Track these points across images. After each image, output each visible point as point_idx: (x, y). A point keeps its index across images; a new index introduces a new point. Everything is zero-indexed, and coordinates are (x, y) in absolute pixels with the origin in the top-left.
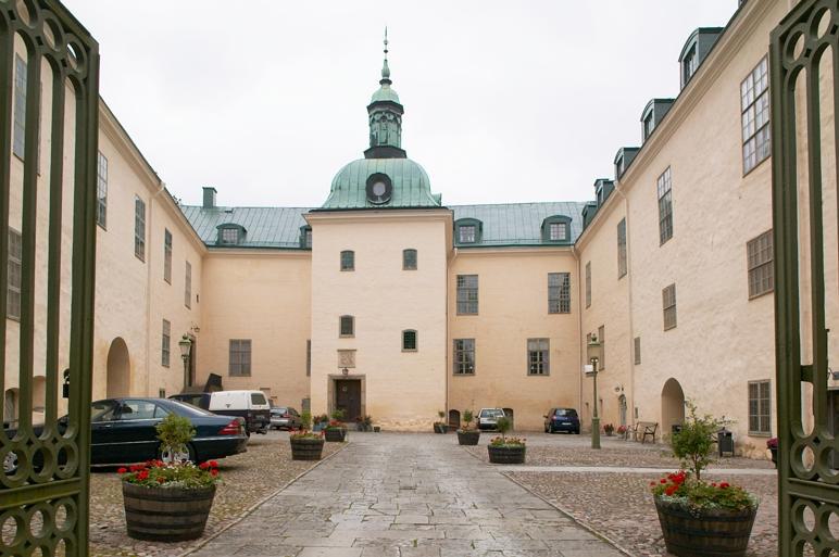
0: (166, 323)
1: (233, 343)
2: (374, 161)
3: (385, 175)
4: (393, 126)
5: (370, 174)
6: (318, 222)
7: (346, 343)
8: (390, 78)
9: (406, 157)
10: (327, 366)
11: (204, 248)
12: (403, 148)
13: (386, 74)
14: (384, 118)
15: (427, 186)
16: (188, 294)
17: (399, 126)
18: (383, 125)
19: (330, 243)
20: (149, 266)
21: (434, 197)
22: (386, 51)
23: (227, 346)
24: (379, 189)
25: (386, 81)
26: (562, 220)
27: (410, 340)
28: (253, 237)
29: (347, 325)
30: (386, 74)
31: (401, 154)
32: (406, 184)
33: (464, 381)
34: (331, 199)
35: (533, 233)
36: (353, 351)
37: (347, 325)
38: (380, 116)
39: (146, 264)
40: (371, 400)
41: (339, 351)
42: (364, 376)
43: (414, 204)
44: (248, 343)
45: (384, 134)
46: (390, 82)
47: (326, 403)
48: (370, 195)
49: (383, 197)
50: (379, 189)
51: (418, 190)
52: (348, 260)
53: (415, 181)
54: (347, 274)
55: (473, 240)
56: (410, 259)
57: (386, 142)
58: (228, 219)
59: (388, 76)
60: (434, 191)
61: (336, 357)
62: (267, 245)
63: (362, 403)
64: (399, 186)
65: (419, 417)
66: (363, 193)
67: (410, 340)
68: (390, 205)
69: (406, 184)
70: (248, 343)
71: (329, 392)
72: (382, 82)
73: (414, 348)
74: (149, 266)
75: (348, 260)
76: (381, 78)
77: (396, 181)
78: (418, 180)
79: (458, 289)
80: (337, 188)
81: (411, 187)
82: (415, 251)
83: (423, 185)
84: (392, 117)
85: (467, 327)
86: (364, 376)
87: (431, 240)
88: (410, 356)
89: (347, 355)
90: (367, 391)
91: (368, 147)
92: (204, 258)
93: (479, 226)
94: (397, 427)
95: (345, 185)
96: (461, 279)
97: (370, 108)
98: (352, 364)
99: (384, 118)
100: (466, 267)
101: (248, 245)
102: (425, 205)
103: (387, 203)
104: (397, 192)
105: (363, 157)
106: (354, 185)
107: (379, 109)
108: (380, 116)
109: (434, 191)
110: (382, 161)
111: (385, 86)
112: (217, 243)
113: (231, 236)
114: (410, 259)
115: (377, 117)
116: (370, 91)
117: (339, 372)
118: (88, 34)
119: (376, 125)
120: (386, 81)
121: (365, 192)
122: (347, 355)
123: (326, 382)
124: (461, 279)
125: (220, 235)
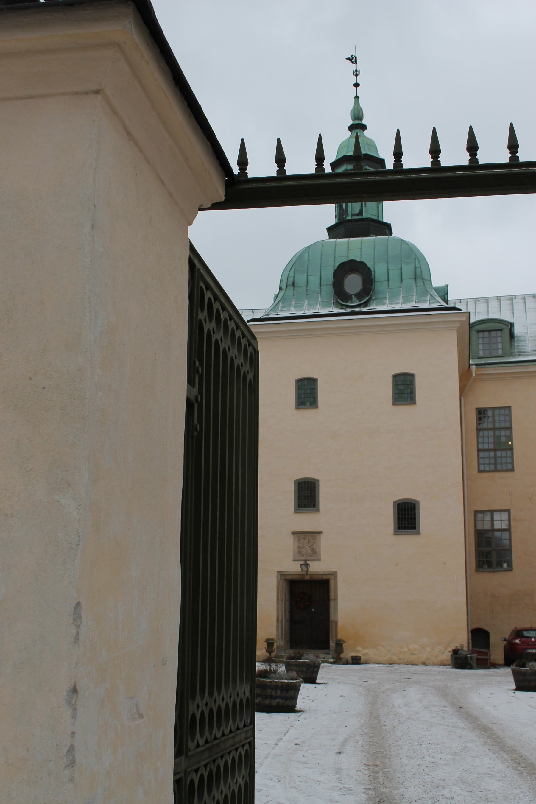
7: (306, 522)
8: (364, 122)
9: (391, 233)
12: (386, 219)
13: (357, 115)
15: (425, 276)
21: (437, 290)
22: (356, 85)
24: (353, 283)
25: (357, 126)
27: (406, 517)
29: (307, 494)
30: (357, 115)
32: (394, 274)
33: (494, 581)
34: (274, 308)
37: (307, 494)
40: (347, 609)
41: (294, 533)
42: (334, 574)
46: (363, 127)
49: (359, 296)
50: (353, 283)
51: (413, 281)
52: (307, 393)
53: (408, 270)
54: (307, 413)
56: (404, 388)
59: (360, 118)
60: (437, 282)
61: (290, 543)
63: (332, 618)
66: (328, 290)
67: (406, 517)
69: (394, 274)
71: (336, 599)
72: (351, 128)
73: (314, 506)
75: (307, 393)
76: (350, 123)
77: (379, 271)
78: (411, 267)
79: (479, 430)
82: (412, 376)
85: (497, 490)
86: (334, 574)
87: (437, 363)
88: (407, 540)
89: (307, 540)
95: (301, 279)
96: (481, 413)
98: (315, 555)
100: (489, 396)
103: (366, 304)
104: (380, 286)
105: (325, 236)
106: (314, 280)
109: (437, 282)
114: (404, 388)
117: (294, 568)
118: (190, 405)
120: (357, 126)
121: (331, 289)
122: (307, 540)
123: (275, 584)
124: (481, 413)
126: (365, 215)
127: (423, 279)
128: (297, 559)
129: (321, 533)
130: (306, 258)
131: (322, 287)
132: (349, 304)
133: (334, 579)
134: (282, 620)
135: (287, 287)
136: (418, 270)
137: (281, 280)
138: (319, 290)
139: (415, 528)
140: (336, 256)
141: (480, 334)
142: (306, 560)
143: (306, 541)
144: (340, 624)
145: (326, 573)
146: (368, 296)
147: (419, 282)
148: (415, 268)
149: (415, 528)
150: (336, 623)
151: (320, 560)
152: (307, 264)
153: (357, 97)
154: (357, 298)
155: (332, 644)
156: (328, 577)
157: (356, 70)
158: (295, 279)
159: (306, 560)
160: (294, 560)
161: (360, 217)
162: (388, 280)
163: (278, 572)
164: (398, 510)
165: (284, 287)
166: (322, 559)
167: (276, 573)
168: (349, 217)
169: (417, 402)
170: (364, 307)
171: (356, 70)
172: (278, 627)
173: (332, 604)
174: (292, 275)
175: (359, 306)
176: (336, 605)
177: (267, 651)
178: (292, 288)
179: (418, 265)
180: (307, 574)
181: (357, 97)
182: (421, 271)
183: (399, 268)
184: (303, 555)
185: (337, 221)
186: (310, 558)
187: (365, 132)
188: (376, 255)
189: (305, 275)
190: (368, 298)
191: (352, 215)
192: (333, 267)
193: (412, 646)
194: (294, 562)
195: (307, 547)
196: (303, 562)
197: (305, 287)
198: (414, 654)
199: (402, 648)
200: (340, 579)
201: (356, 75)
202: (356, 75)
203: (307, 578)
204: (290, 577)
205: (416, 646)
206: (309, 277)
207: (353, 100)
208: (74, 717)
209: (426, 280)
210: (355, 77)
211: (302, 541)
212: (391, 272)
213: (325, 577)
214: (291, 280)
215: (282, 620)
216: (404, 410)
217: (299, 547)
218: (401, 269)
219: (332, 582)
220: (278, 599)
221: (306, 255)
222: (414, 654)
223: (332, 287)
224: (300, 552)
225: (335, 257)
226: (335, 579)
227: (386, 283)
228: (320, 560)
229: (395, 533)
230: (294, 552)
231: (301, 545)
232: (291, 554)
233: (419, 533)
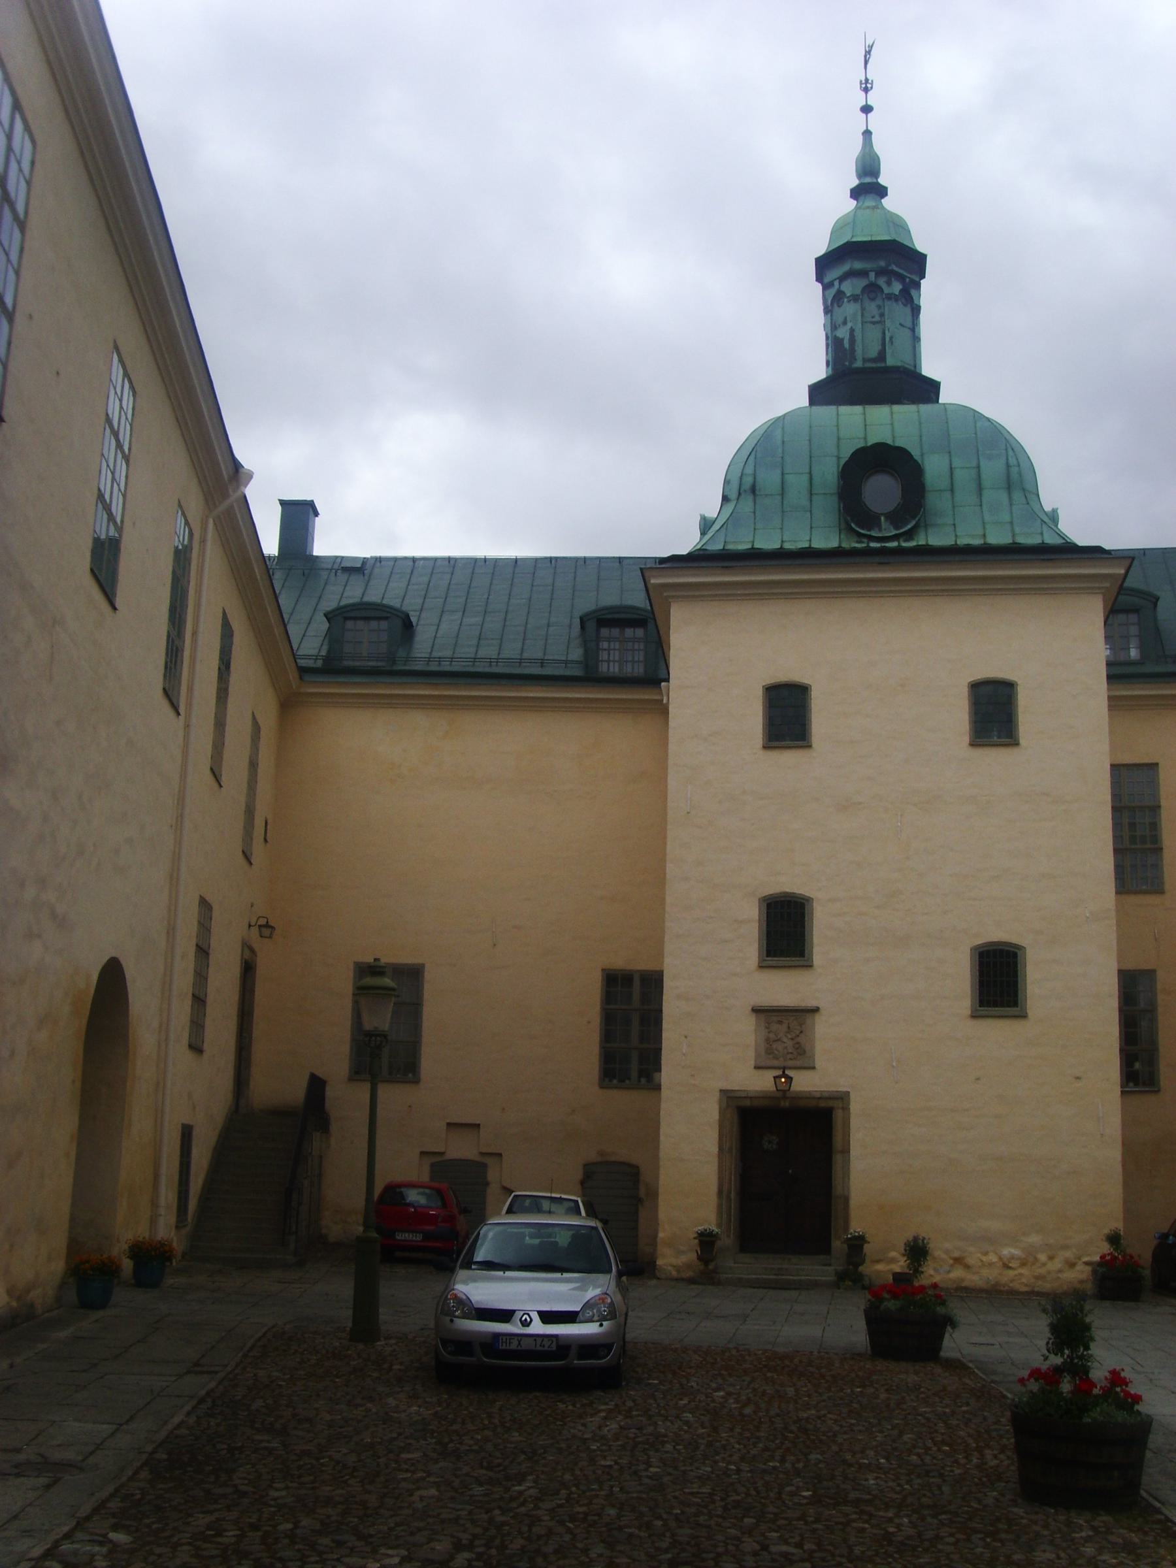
0: (205, 905)
1: (369, 970)
2: (851, 414)
3: (903, 453)
4: (899, 312)
5: (846, 454)
6: (693, 593)
7: (783, 988)
10: (709, 1055)
11: (293, 675)
12: (929, 369)
14: (872, 290)
16: (250, 812)
17: (916, 310)
18: (872, 307)
19: (718, 660)
20: (187, 726)
23: (345, 983)
25: (869, 188)
26: (385, 615)
27: (998, 978)
28: (433, 639)
29: (786, 928)
31: (928, 390)
32: (963, 476)
35: (564, 648)
36: (803, 1015)
37: (786, 928)
38: (861, 283)
39: (182, 718)
40: (876, 1172)
41: (757, 1011)
42: (843, 1098)
43: (997, 538)
44: (413, 975)
45: (874, 334)
46: (882, 192)
47: (714, 1188)
48: (851, 505)
49: (895, 518)
50: (881, 491)
51: (1003, 496)
52: (787, 715)
53: (992, 470)
55: (1134, 653)
56: (994, 712)
57: (882, 356)
58: (353, 593)
59: (875, 173)
61: (747, 1030)
62: (480, 668)
63: (838, 1189)
64: (945, 483)
65: (1034, 1239)
66: (827, 508)
67: (998, 978)
68: (920, 540)
70: (413, 975)
71: (846, 1151)
72: (856, 193)
74: (187, 726)
75: (787, 715)
76: (855, 182)
77: (934, 468)
78: (1000, 465)
80: (746, 486)
81: (980, 489)
83: (1018, 479)
84: (897, 287)
86: (843, 1098)
87: (1059, 653)
88: (997, 1032)
89: (786, 1029)
90: (855, 1151)
91: (819, 371)
92: (289, 704)
93: (405, 626)
94: (958, 1273)
95: (769, 479)
97: (824, 264)
98: (802, 1056)
99: (872, 290)
101: (419, 667)
102: (1035, 540)
103: (909, 535)
104: (936, 501)
106: (797, 483)
107: (858, 265)
108: (861, 283)
110: (880, 414)
111: (869, 202)
112: (327, 659)
113: (367, 641)
114: (994, 712)
115: (848, 287)
116: (823, 208)
117: (762, 1083)
119: (849, 309)
120: (869, 188)
122: (786, 1029)
123: (715, 1115)
125: (333, 638)
126: (890, 361)
127: (1024, 490)
128: (763, 1064)
129: (816, 1010)
130: (779, 437)
131: (814, 497)
132: (873, 533)
133: (843, 1108)
134: (729, 1192)
135: (740, 494)
136: (1014, 470)
137: (727, 482)
138: (808, 503)
139: (1016, 1004)
140: (841, 436)
141: (605, 632)
142: (784, 1069)
143: (784, 1027)
144: (853, 1203)
145: (825, 1095)
146: (913, 517)
147: (1017, 496)
148: (1008, 466)
149: (1016, 1004)
150: (847, 1199)
151: (814, 1068)
152: (780, 450)
153: (867, 134)
154: (891, 523)
155: (837, 1245)
156: (831, 1104)
157: (867, 80)
158: (758, 479)
159: (784, 1069)
160: (757, 1068)
161: (879, 365)
162: (952, 490)
163: (721, 1091)
164: (981, 964)
165: (733, 495)
166: (818, 1064)
167: (718, 1094)
168: (859, 364)
169: (1022, 741)
170: (905, 541)
171: (867, 80)
172: (720, 1206)
173: (838, 1159)
174: (749, 470)
175: (895, 538)
176: (847, 1162)
177: (699, 1258)
178: (750, 498)
179: (1012, 461)
180: (784, 1097)
181: (867, 134)
182: (1020, 473)
183: (974, 464)
184: (776, 1058)
185: (830, 372)
186: (790, 1063)
187: (885, 202)
188: (924, 439)
189: (779, 472)
190: (913, 523)
191: (865, 360)
192: (835, 459)
193: (1006, 1252)
194: (760, 1072)
195: (785, 1040)
196: (780, 1072)
197: (779, 498)
198: (1010, 1268)
199: (986, 1254)
200: (855, 1107)
201: (866, 90)
202: (866, 90)
203: (785, 1104)
204: (748, 1103)
205: (1016, 1252)
206: (786, 476)
207: (859, 140)
208: (872, 271)
209: (1030, 492)
210: (863, 94)
211: (775, 1027)
212: (958, 474)
213: (823, 1104)
214: (748, 480)
215: (729, 1192)
216: (994, 758)
217: (767, 1040)
218: (978, 467)
219: (838, 1115)
220: (721, 1149)
221: (778, 433)
222: (1010, 1268)
223: (835, 498)
224: (769, 1051)
225: (839, 439)
226: (846, 1109)
227: (948, 495)
228: (814, 1068)
229: (974, 1016)
230: (756, 1051)
231: (772, 1036)
232: (751, 1054)
233: (1023, 1016)
